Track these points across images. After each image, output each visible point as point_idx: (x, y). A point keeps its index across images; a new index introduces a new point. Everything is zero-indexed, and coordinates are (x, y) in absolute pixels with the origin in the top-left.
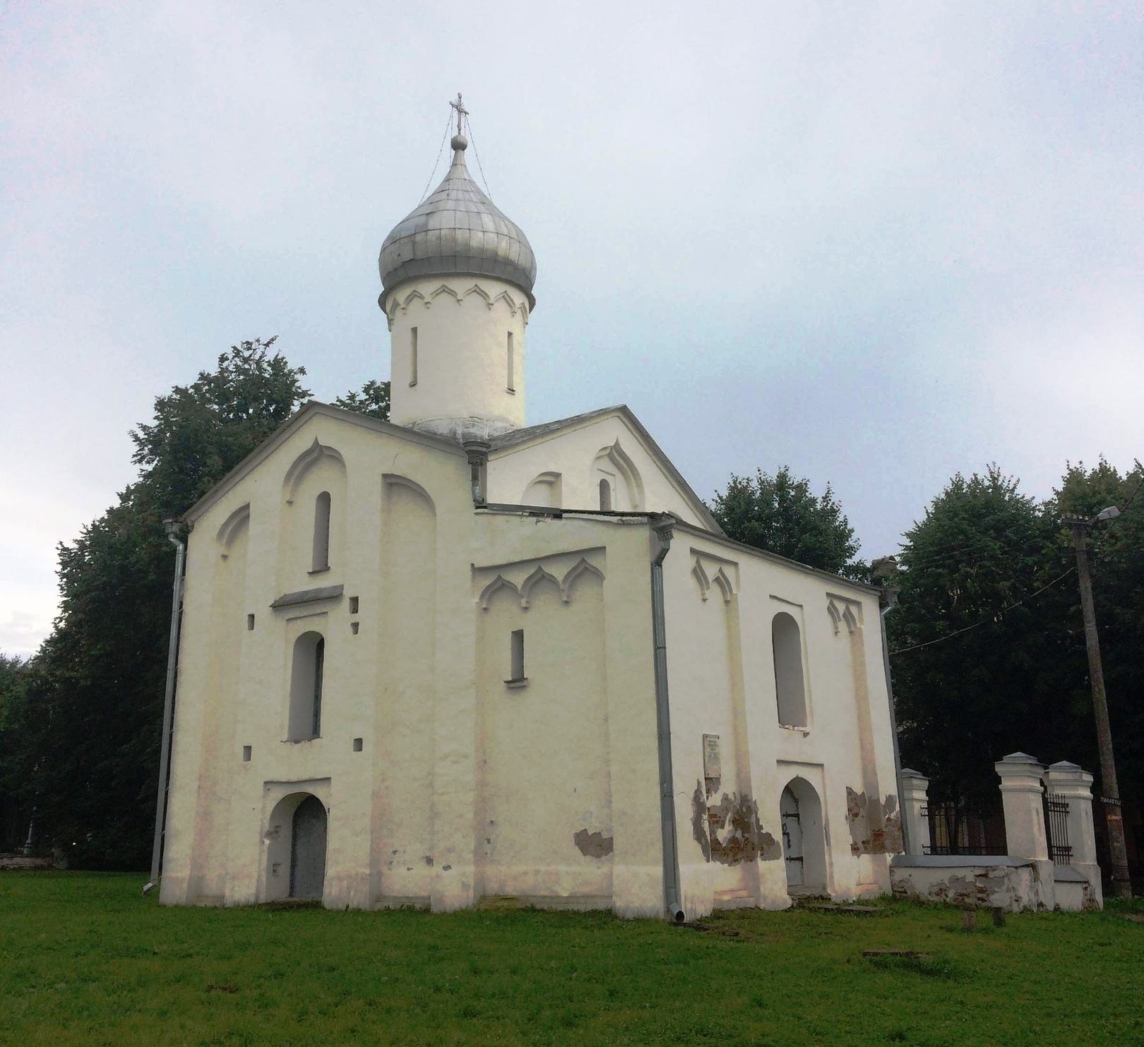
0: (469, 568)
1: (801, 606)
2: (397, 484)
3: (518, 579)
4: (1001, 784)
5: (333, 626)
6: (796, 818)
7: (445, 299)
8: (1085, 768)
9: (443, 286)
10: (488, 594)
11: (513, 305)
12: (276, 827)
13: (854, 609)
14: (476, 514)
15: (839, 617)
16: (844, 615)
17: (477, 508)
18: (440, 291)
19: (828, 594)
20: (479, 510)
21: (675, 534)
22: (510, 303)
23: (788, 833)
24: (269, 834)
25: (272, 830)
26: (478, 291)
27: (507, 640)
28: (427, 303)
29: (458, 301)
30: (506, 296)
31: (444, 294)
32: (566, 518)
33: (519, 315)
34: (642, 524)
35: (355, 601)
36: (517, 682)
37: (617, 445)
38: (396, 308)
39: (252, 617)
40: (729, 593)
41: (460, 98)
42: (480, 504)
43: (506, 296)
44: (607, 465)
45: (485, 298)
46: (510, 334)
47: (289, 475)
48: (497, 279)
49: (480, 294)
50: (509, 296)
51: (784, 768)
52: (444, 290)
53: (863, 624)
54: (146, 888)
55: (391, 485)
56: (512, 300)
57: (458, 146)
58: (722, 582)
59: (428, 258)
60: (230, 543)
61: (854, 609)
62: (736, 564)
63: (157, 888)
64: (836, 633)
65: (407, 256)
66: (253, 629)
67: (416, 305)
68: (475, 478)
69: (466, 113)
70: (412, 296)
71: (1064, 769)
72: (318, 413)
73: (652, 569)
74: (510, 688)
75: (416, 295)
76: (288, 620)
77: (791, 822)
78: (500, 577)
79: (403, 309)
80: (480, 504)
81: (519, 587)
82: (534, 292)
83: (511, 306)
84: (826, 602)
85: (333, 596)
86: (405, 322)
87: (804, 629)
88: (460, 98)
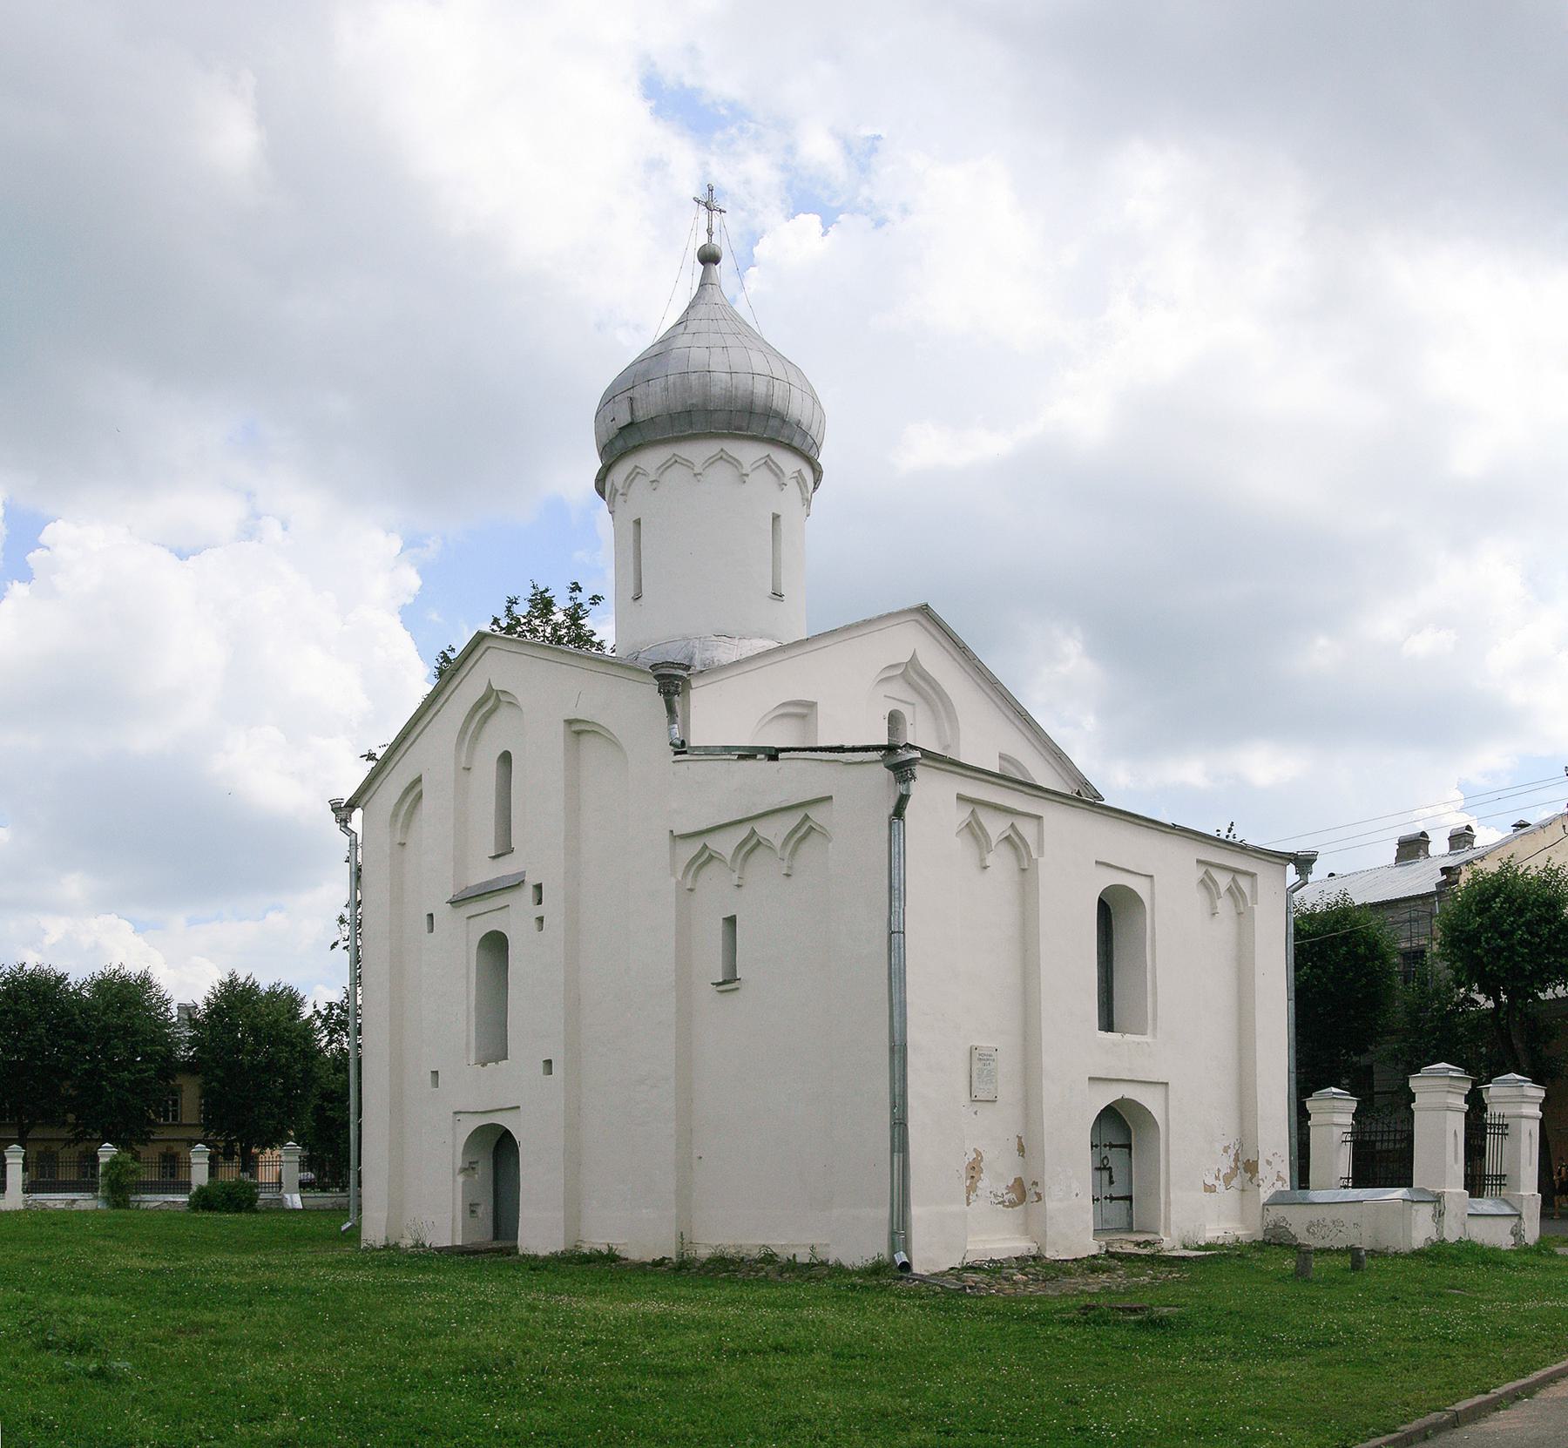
0: (668, 833)
1: (1151, 876)
3: (725, 844)
4: (1414, 1102)
5: (515, 919)
6: (1127, 1150)
8: (1537, 1080)
11: (781, 475)
13: (1244, 883)
14: (674, 762)
15: (1218, 893)
16: (1229, 889)
17: (676, 753)
19: (1199, 861)
20: (679, 757)
21: (918, 770)
22: (777, 472)
23: (1110, 1168)
24: (463, 1170)
26: (768, 463)
27: (718, 927)
33: (792, 486)
35: (539, 887)
36: (729, 980)
37: (913, 660)
38: (615, 495)
39: (431, 916)
42: (681, 748)
44: (899, 690)
46: (776, 518)
48: (754, 438)
49: (728, 462)
50: (774, 463)
51: (1102, 1087)
53: (1256, 904)
54: (344, 1228)
55: (578, 733)
58: (1013, 842)
59: (652, 418)
60: (407, 826)
61: (1244, 883)
62: (1039, 818)
63: (357, 1228)
65: (624, 419)
66: (432, 932)
68: (671, 710)
70: (633, 475)
71: (1511, 1083)
72: (489, 647)
75: (638, 473)
76: (469, 918)
77: (1115, 1158)
78: (705, 847)
79: (622, 494)
81: (728, 858)
83: (776, 475)
84: (1199, 873)
87: (1153, 905)
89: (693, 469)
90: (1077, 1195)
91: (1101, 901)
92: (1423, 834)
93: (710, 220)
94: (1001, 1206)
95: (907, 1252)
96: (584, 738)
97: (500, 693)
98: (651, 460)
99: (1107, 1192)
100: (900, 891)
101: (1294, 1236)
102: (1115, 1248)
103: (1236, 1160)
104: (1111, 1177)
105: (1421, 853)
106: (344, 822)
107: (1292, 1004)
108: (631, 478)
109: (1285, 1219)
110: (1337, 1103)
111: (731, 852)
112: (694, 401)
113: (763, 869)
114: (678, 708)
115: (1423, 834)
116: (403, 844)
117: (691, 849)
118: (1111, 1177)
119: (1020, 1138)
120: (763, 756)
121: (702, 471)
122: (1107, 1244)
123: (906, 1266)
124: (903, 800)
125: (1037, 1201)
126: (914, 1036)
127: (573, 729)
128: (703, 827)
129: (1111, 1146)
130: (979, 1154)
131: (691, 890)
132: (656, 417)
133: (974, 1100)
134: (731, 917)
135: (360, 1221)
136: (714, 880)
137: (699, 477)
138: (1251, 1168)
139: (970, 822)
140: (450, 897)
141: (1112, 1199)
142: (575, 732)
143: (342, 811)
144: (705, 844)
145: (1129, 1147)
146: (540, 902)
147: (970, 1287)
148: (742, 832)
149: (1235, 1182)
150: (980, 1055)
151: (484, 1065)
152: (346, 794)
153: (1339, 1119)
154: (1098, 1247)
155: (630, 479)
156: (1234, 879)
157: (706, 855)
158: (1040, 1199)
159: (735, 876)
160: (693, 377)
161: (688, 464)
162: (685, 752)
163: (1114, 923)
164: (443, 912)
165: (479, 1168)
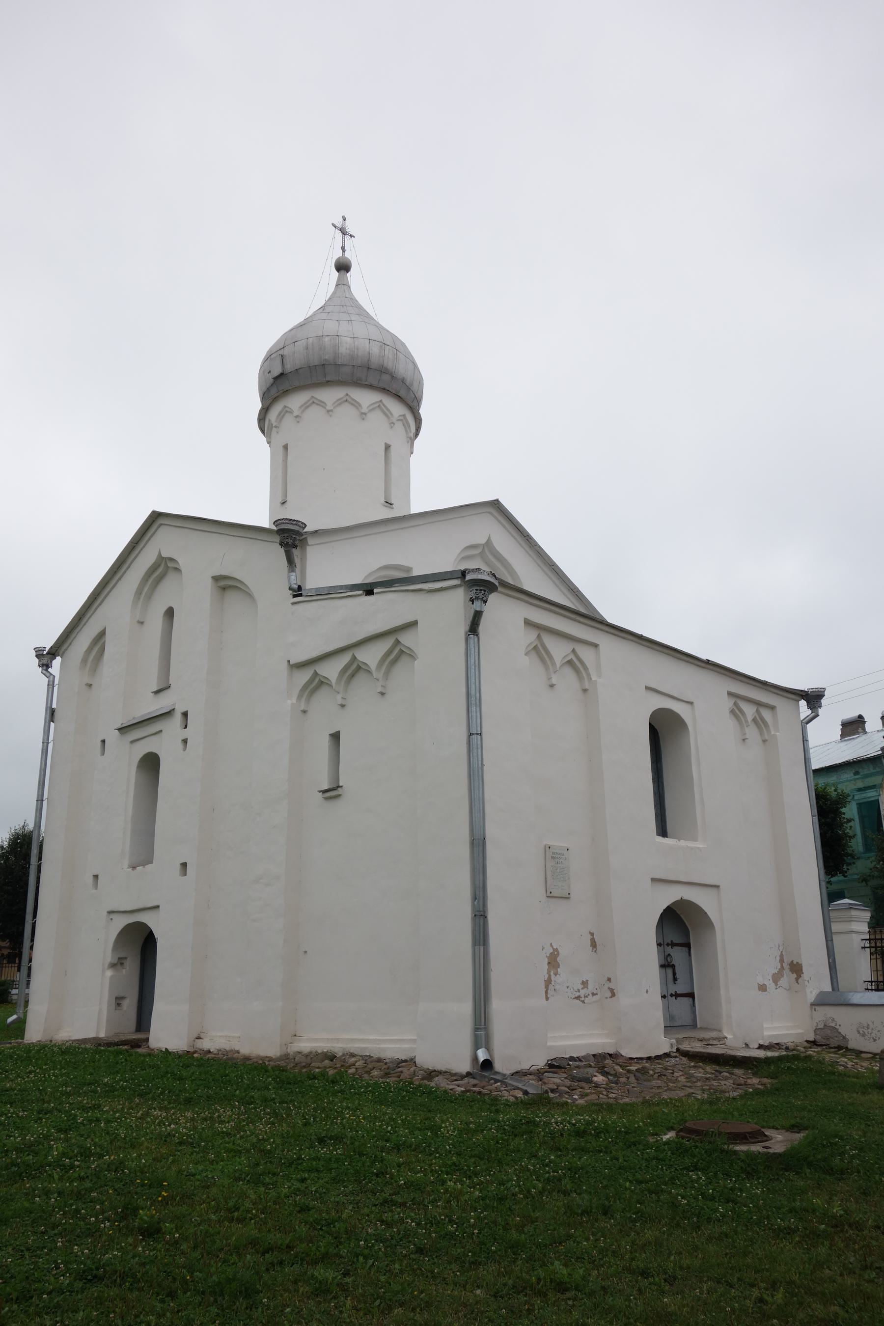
0: (286, 664)
1: (691, 703)
2: (230, 587)
3: (331, 670)
6: (685, 949)
7: (315, 412)
9: (313, 397)
10: (306, 693)
12: (119, 959)
13: (766, 714)
14: (293, 604)
15: (746, 721)
17: (295, 596)
18: (309, 403)
22: (387, 414)
24: (113, 966)
25: (115, 961)
27: (325, 742)
28: (297, 417)
29: (328, 411)
30: (381, 405)
31: (314, 406)
32: (377, 593)
34: (455, 587)
35: (185, 715)
36: (332, 792)
37: (489, 543)
39: (103, 741)
40: (586, 680)
41: (344, 220)
42: (298, 592)
43: (381, 405)
45: (357, 408)
46: (387, 447)
47: (139, 592)
48: (371, 387)
52: (314, 402)
55: (224, 589)
56: (388, 410)
57: (343, 267)
58: (574, 664)
61: (766, 714)
62: (596, 646)
64: (744, 740)
65: (277, 371)
67: (288, 420)
68: (290, 561)
69: (351, 236)
72: (161, 525)
73: (467, 640)
74: (326, 799)
75: (287, 411)
76: (132, 742)
77: (677, 955)
78: (316, 674)
80: (298, 592)
82: (423, 411)
83: (387, 416)
84: (729, 703)
85: (169, 714)
86: (280, 439)
88: (344, 220)
89: (325, 408)
90: (647, 992)
91: (651, 725)
92: (860, 717)
93: (344, 241)
94: (577, 1001)
95: (488, 1049)
96: (232, 598)
97: (167, 561)
98: (295, 401)
99: (673, 989)
100: (476, 698)
101: (844, 1038)
102: (686, 1047)
103: (782, 961)
104: (674, 974)
105: (860, 730)
106: (45, 666)
107: (816, 819)
108: (282, 415)
109: (833, 1020)
110: (854, 913)
111: (336, 675)
112: (327, 357)
113: (362, 688)
114: (297, 560)
115: (860, 717)
116: (90, 686)
117: (304, 676)
118: (674, 974)
119: (592, 934)
120: (361, 592)
121: (332, 408)
122: (677, 1042)
123: (487, 1065)
124: (478, 615)
125: (611, 997)
126: (492, 831)
127: (218, 585)
128: (314, 654)
129: (673, 945)
130: (797, 982)
131: (304, 712)
132: (300, 369)
133: (550, 896)
134: (337, 732)
135: (25, 1013)
136: (324, 702)
137: (331, 413)
138: (796, 969)
139: (536, 645)
140: (119, 726)
141: (677, 995)
142: (220, 587)
143: (45, 658)
144: (315, 670)
145: (688, 946)
146: (186, 727)
147: (553, 1091)
148: (345, 659)
149: (783, 982)
150: (553, 853)
151: (134, 868)
152: (48, 643)
153: (855, 926)
154: (669, 1045)
155: (281, 416)
156: (757, 711)
157: (317, 680)
158: (613, 995)
159: (339, 697)
160: (327, 339)
161: (322, 404)
162: (301, 595)
163: (661, 743)
164: (113, 736)
165: (127, 963)
